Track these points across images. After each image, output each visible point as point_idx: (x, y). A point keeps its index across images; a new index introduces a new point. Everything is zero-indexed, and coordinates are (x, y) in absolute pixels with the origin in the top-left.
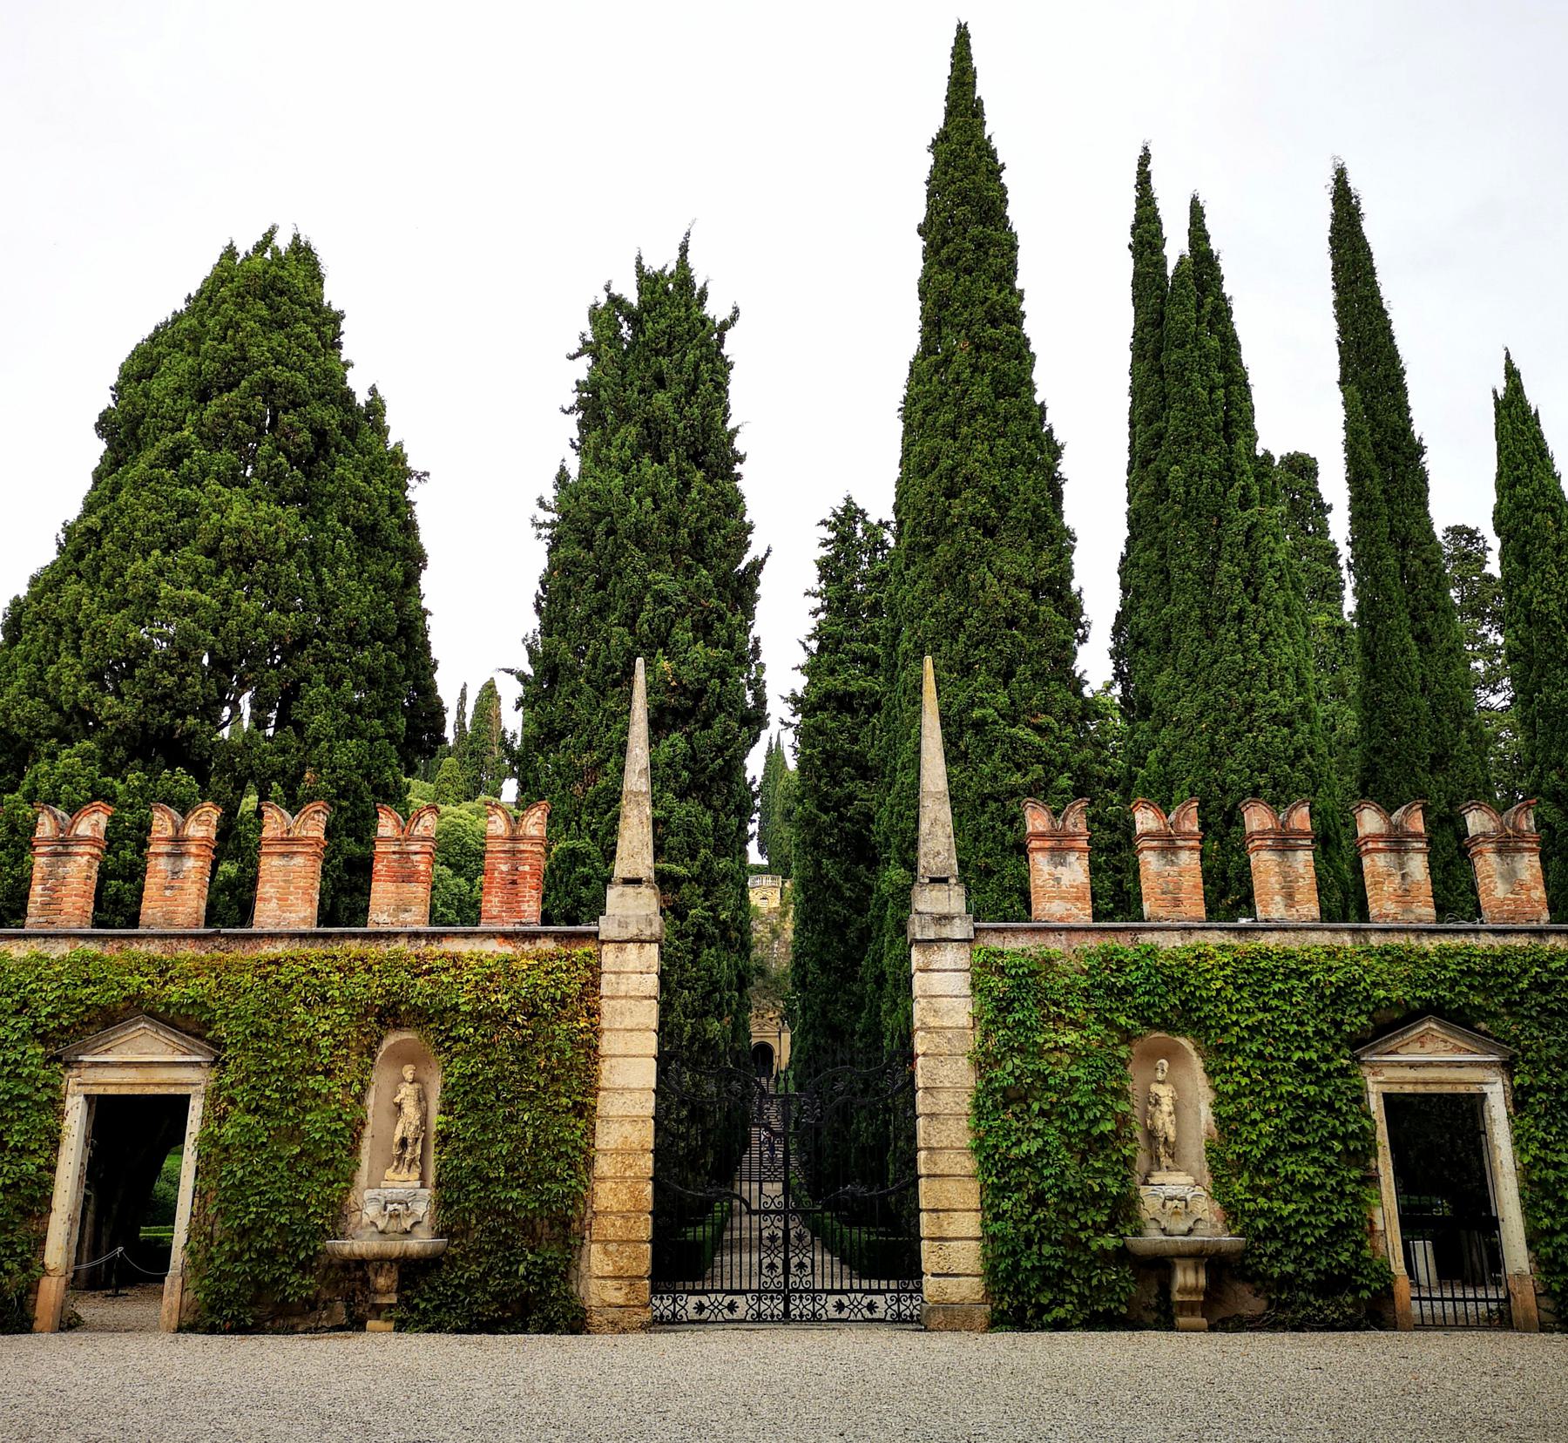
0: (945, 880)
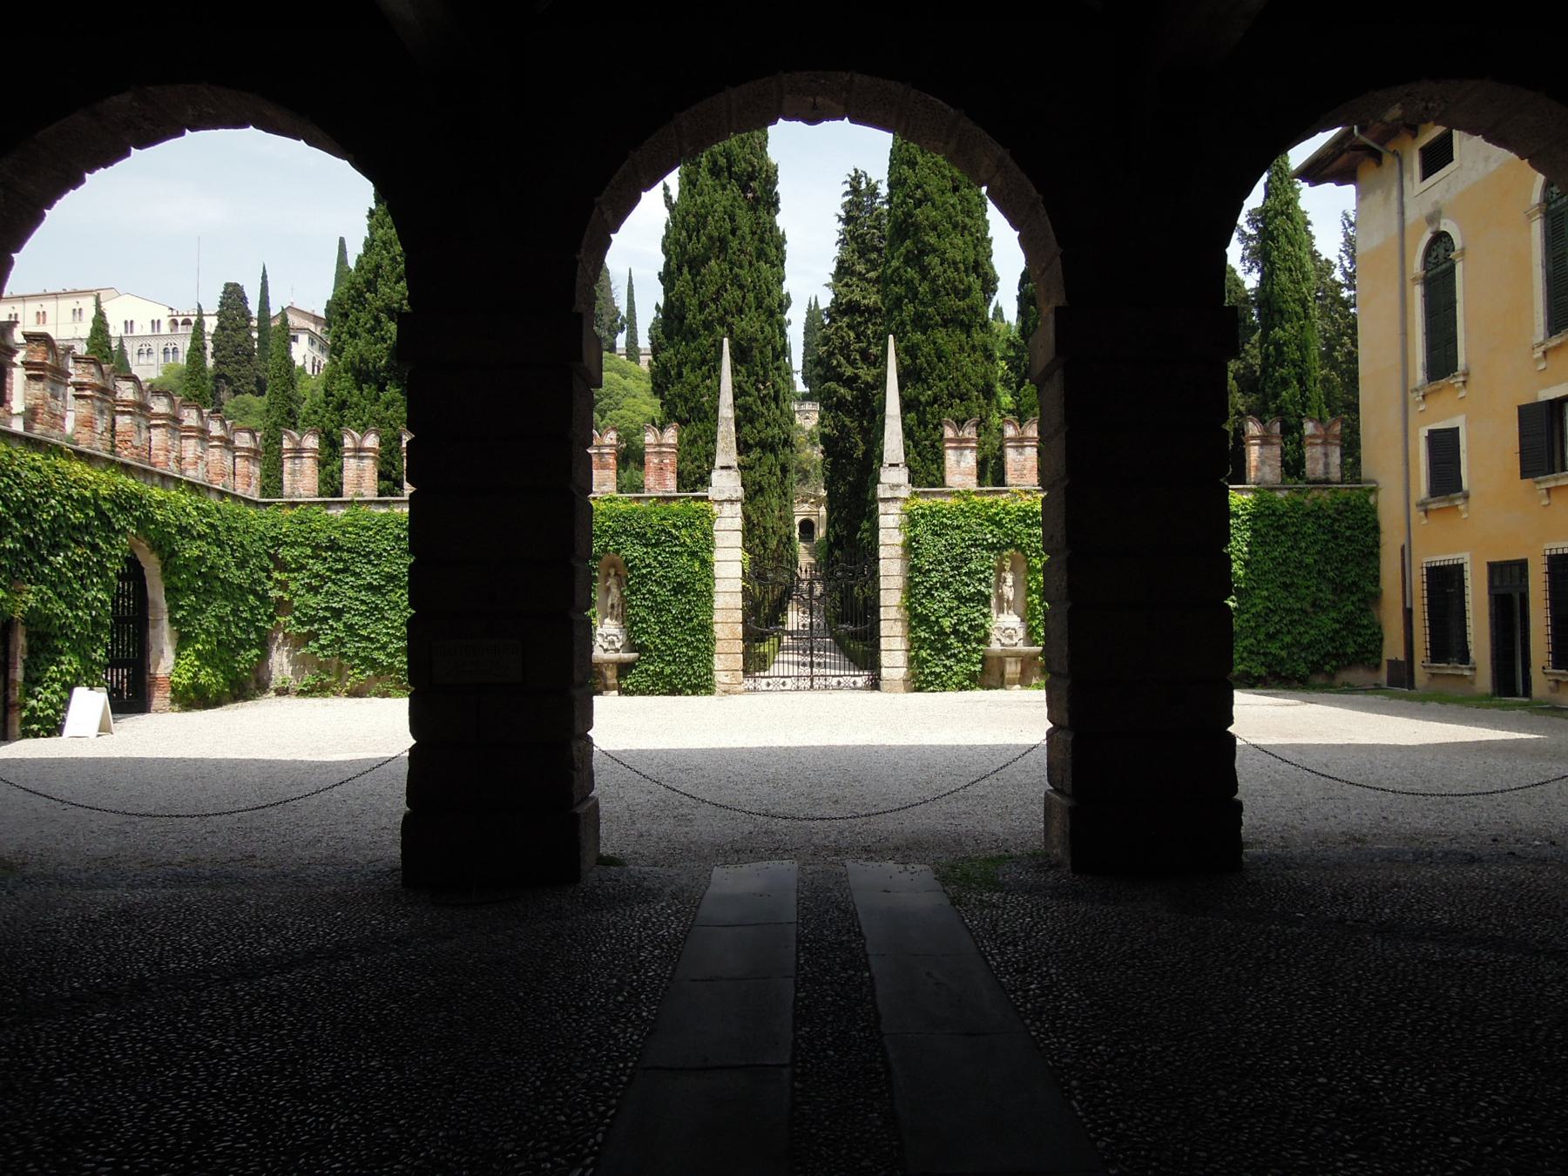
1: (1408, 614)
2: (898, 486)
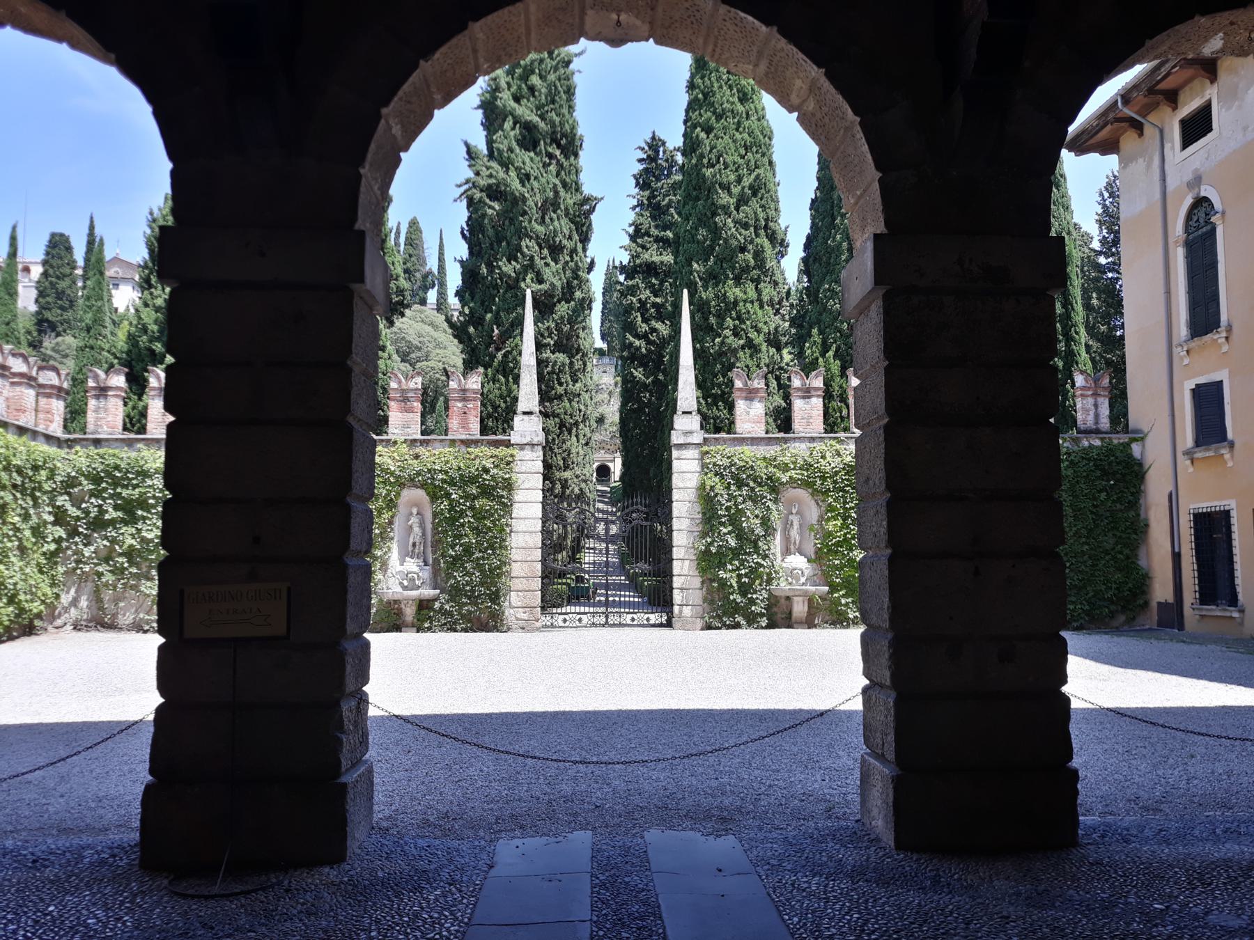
0: (690, 413)
1: (1177, 557)
2: (691, 432)
